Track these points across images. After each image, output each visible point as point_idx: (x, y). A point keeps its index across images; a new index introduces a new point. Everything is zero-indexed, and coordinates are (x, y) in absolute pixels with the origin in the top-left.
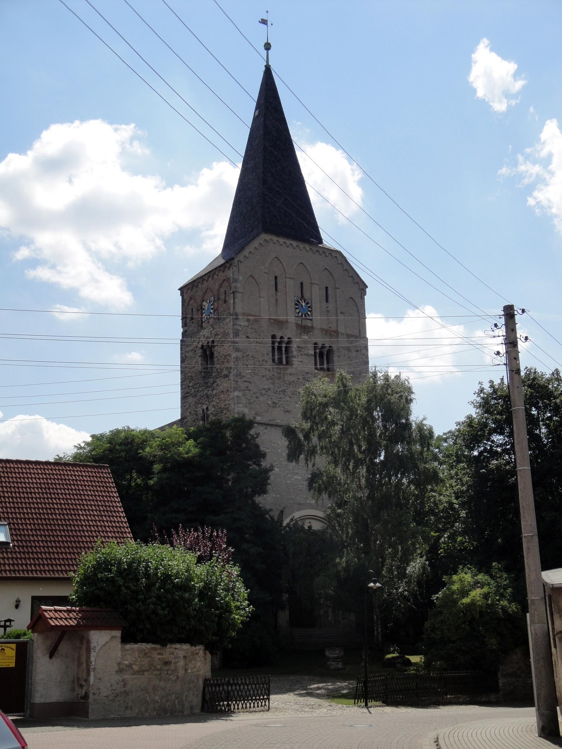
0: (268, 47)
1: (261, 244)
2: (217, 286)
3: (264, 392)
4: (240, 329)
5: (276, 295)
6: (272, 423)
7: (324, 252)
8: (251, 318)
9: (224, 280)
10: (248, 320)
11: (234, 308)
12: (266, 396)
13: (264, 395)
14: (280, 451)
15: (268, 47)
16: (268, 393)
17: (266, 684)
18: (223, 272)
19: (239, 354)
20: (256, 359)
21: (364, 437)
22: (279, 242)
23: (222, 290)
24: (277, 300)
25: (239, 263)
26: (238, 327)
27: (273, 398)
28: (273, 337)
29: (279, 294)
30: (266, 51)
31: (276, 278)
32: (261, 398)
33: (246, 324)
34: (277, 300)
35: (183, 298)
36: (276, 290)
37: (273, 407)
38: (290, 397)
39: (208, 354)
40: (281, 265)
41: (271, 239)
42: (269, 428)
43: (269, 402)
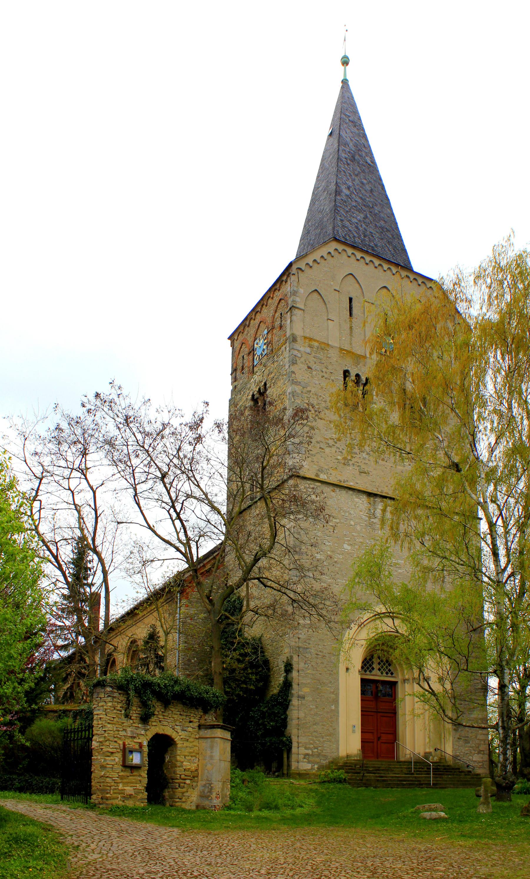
0: (345, 62)
1: (329, 253)
2: (272, 312)
3: (331, 442)
4: (299, 355)
5: (351, 321)
6: (342, 484)
7: (415, 279)
8: (316, 344)
9: (281, 300)
10: (310, 346)
11: (291, 328)
12: (334, 449)
13: (330, 447)
14: (352, 523)
15: (345, 62)
16: (338, 445)
17: (85, 731)
18: (279, 290)
19: (298, 389)
20: (320, 399)
21: (484, 405)
22: (355, 256)
23: (278, 314)
24: (351, 328)
25: (300, 272)
26: (295, 352)
27: (344, 452)
28: (346, 373)
29: (354, 320)
30: (343, 67)
31: (351, 300)
32: (327, 450)
33: (308, 350)
34: (351, 328)
35: (233, 348)
36: (351, 315)
37: (344, 464)
38: (368, 454)
39: (260, 400)
40: (357, 285)
41: (345, 251)
42: (337, 490)
43: (339, 457)
